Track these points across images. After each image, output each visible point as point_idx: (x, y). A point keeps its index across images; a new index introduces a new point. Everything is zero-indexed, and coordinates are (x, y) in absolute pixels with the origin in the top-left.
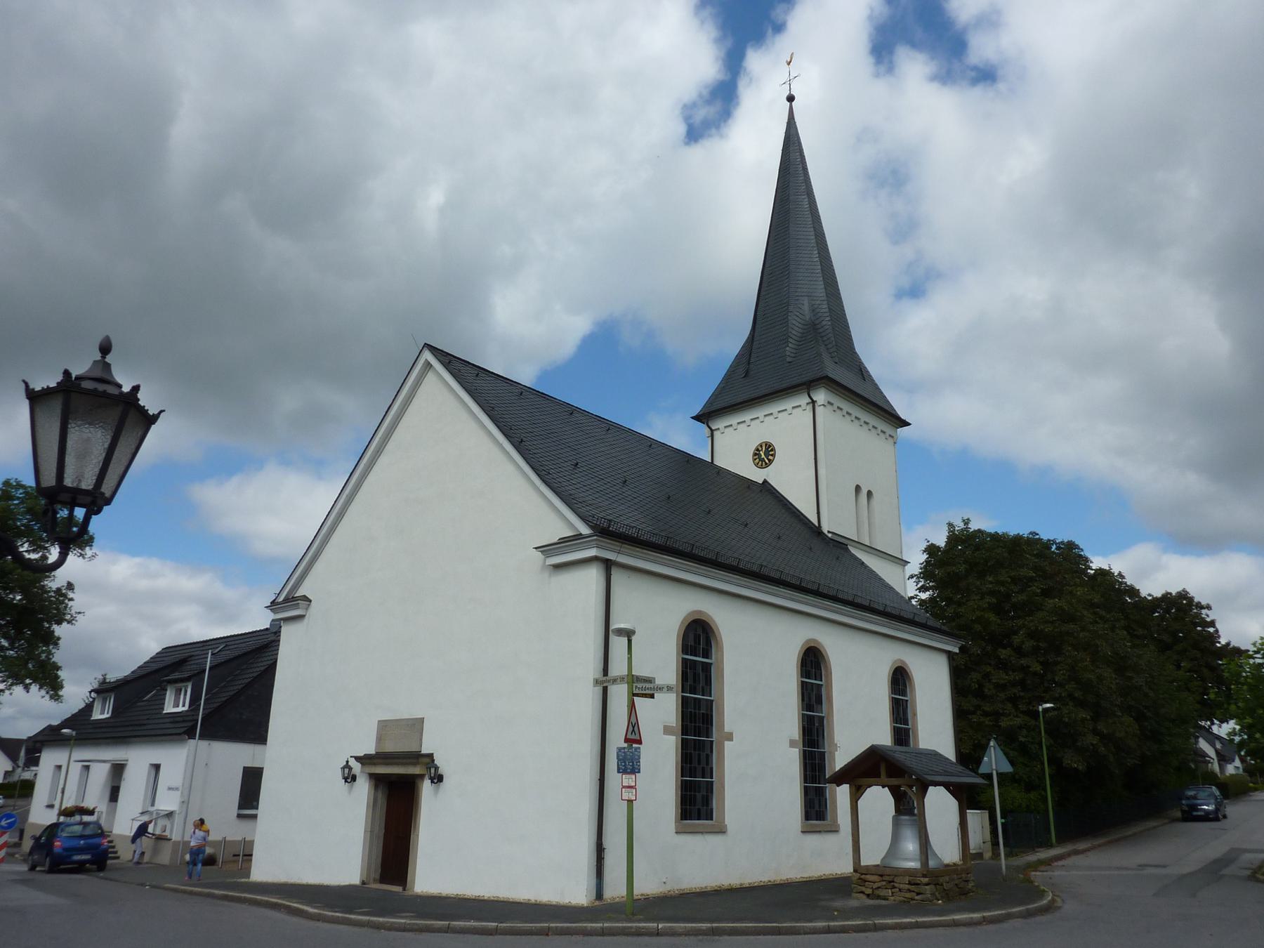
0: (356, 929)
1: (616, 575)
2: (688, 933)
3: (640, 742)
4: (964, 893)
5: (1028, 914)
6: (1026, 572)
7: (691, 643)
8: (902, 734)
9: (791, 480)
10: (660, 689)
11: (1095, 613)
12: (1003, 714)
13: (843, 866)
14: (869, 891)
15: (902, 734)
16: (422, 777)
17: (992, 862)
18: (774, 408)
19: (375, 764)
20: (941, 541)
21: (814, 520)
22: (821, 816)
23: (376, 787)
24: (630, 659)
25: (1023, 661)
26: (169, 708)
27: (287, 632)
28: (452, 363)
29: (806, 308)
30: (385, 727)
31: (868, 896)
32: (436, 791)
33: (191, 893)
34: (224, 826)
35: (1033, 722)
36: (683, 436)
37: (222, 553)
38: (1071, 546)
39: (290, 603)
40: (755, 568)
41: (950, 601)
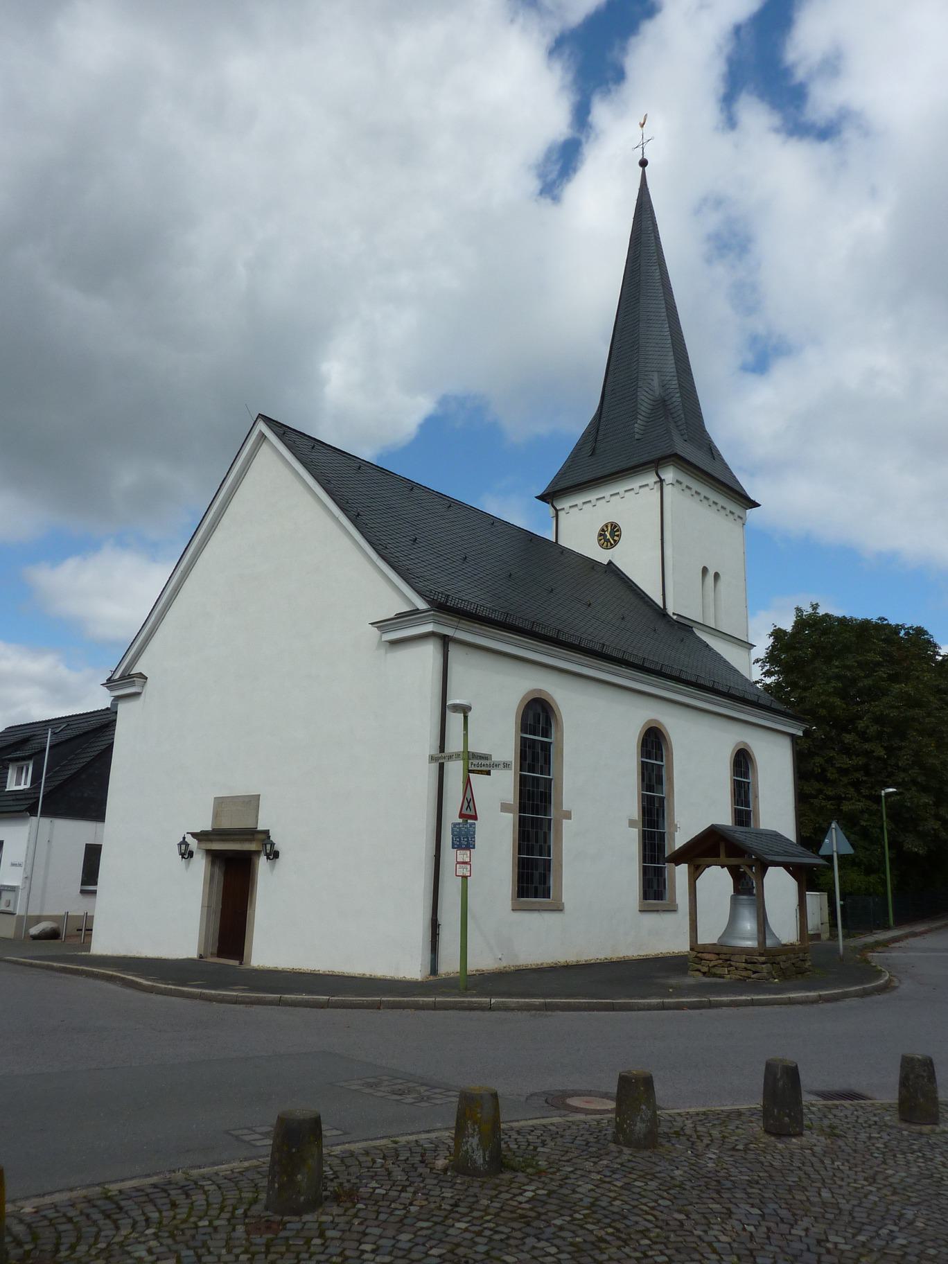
0: (187, 1001)
1: (454, 651)
2: (521, 1008)
3: (475, 818)
4: (801, 972)
5: (865, 994)
6: (871, 656)
7: (530, 721)
8: (743, 814)
9: (637, 561)
10: (496, 765)
11: (941, 699)
12: (845, 799)
13: (681, 945)
14: (705, 969)
15: (743, 814)
16: (258, 853)
17: (830, 943)
18: (620, 488)
19: (211, 841)
20: (788, 625)
21: (660, 602)
22: (659, 895)
23: (213, 863)
24: (466, 735)
25: (867, 746)
26: (11, 786)
27: (122, 708)
28: (285, 433)
29: (656, 383)
31: (704, 973)
32: (273, 867)
33: (31, 965)
34: (60, 898)
35: (875, 807)
36: (518, 510)
37: (57, 633)
38: (920, 631)
39: (126, 681)
40: (597, 647)
41: (794, 685)
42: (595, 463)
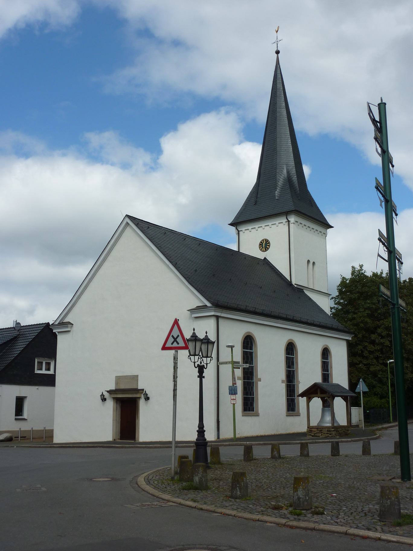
1: (221, 321)
8: (326, 377)
9: (277, 258)
12: (372, 365)
13: (304, 429)
14: (313, 434)
15: (326, 377)
16: (139, 398)
19: (116, 394)
21: (289, 279)
23: (117, 403)
24: (232, 356)
29: (285, 171)
30: (118, 379)
33: (40, 447)
35: (385, 368)
36: (228, 239)
42: (257, 208)
